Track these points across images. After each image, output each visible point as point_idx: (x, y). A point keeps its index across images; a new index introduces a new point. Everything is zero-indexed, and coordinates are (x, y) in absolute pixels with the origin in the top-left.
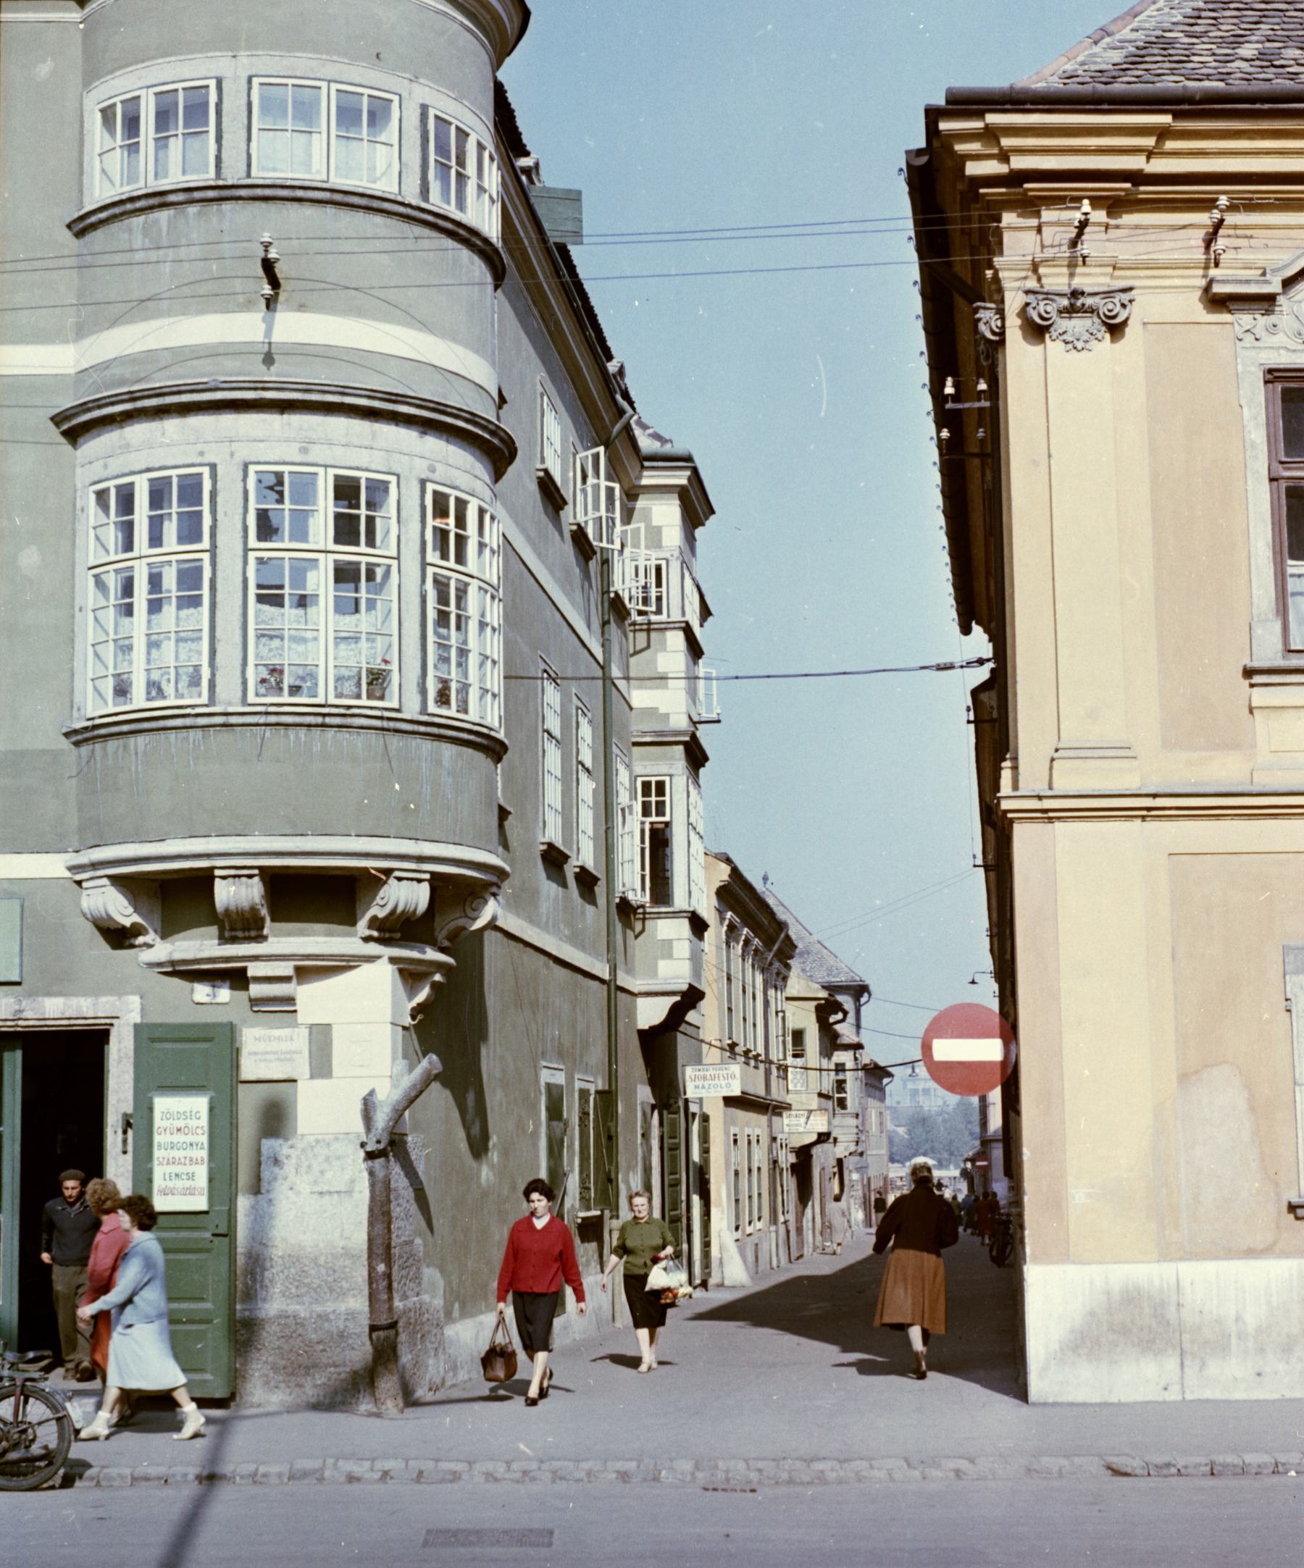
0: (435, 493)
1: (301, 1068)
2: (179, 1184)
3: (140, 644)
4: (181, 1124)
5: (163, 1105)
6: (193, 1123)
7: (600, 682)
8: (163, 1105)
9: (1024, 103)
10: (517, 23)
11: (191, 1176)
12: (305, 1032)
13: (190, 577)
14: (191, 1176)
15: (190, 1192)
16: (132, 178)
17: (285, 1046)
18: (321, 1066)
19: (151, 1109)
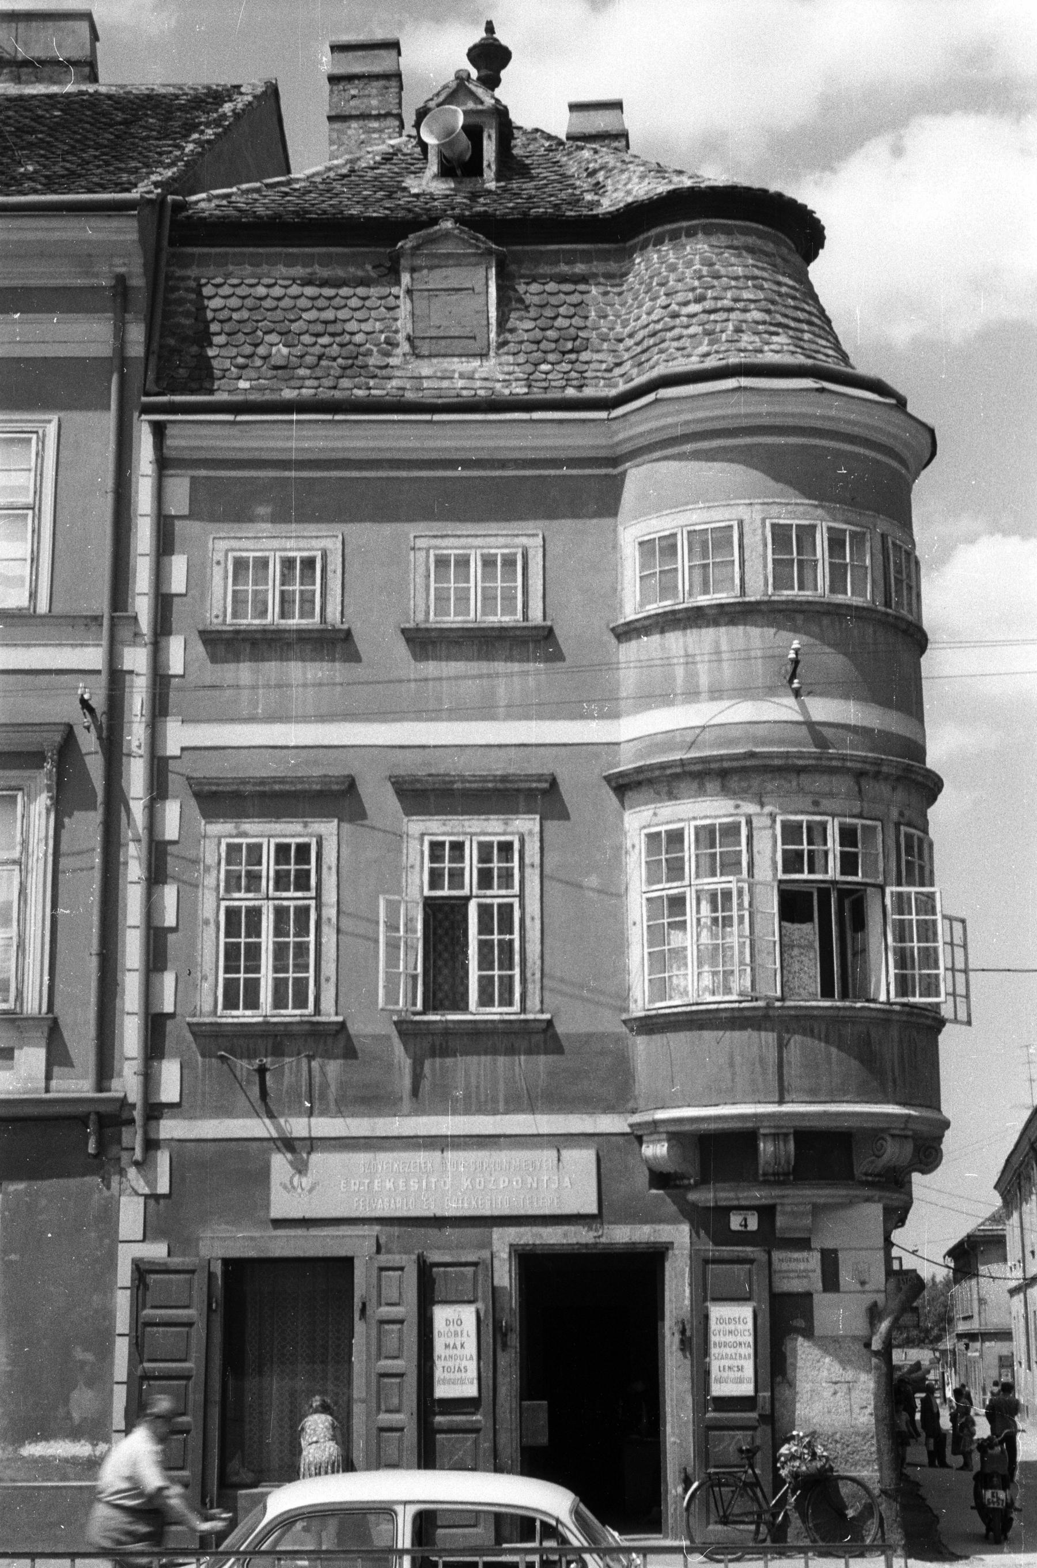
0: (906, 834)
1: (816, 1282)
2: (732, 1375)
3: (267, 884)
4: (732, 1327)
5: (718, 1312)
6: (740, 1327)
7: (971, 967)
8: (718, 1312)
9: (743, 612)
10: (928, 456)
11: (740, 1369)
12: (817, 1255)
13: (452, 873)
14: (740, 1369)
15: (740, 1381)
16: (668, 589)
17: (802, 1266)
18: (831, 1282)
19: (707, 1317)
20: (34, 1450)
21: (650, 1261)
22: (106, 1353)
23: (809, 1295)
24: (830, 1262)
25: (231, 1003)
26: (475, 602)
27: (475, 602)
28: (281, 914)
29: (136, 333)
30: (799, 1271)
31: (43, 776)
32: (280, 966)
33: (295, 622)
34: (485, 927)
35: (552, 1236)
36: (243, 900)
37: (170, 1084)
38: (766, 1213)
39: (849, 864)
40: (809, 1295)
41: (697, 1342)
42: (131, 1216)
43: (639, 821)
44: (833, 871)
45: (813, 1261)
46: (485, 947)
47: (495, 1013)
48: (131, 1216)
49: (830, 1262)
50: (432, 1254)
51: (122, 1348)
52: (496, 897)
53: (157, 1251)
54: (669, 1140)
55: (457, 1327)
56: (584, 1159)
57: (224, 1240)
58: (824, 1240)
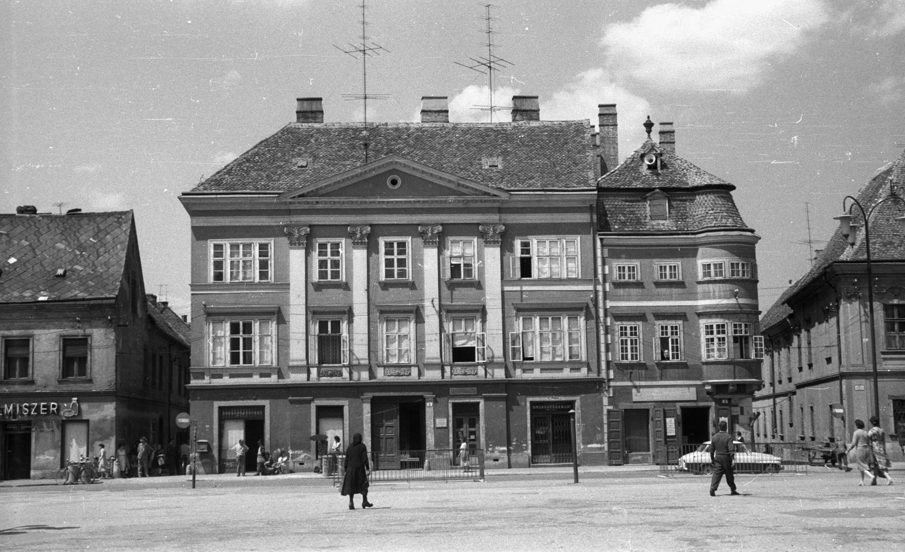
18: (742, 413)
20: (590, 446)
21: (707, 409)
22: (602, 427)
23: (737, 416)
25: (623, 359)
28: (632, 341)
29: (595, 217)
32: (632, 351)
34: (672, 343)
36: (624, 338)
37: (612, 376)
38: (729, 400)
40: (737, 416)
42: (605, 401)
44: (743, 334)
47: (675, 360)
48: (605, 401)
49: (742, 409)
50: (665, 408)
51: (606, 427)
52: (675, 337)
53: (611, 408)
55: (671, 422)
56: (693, 389)
57: (624, 405)
58: (740, 405)
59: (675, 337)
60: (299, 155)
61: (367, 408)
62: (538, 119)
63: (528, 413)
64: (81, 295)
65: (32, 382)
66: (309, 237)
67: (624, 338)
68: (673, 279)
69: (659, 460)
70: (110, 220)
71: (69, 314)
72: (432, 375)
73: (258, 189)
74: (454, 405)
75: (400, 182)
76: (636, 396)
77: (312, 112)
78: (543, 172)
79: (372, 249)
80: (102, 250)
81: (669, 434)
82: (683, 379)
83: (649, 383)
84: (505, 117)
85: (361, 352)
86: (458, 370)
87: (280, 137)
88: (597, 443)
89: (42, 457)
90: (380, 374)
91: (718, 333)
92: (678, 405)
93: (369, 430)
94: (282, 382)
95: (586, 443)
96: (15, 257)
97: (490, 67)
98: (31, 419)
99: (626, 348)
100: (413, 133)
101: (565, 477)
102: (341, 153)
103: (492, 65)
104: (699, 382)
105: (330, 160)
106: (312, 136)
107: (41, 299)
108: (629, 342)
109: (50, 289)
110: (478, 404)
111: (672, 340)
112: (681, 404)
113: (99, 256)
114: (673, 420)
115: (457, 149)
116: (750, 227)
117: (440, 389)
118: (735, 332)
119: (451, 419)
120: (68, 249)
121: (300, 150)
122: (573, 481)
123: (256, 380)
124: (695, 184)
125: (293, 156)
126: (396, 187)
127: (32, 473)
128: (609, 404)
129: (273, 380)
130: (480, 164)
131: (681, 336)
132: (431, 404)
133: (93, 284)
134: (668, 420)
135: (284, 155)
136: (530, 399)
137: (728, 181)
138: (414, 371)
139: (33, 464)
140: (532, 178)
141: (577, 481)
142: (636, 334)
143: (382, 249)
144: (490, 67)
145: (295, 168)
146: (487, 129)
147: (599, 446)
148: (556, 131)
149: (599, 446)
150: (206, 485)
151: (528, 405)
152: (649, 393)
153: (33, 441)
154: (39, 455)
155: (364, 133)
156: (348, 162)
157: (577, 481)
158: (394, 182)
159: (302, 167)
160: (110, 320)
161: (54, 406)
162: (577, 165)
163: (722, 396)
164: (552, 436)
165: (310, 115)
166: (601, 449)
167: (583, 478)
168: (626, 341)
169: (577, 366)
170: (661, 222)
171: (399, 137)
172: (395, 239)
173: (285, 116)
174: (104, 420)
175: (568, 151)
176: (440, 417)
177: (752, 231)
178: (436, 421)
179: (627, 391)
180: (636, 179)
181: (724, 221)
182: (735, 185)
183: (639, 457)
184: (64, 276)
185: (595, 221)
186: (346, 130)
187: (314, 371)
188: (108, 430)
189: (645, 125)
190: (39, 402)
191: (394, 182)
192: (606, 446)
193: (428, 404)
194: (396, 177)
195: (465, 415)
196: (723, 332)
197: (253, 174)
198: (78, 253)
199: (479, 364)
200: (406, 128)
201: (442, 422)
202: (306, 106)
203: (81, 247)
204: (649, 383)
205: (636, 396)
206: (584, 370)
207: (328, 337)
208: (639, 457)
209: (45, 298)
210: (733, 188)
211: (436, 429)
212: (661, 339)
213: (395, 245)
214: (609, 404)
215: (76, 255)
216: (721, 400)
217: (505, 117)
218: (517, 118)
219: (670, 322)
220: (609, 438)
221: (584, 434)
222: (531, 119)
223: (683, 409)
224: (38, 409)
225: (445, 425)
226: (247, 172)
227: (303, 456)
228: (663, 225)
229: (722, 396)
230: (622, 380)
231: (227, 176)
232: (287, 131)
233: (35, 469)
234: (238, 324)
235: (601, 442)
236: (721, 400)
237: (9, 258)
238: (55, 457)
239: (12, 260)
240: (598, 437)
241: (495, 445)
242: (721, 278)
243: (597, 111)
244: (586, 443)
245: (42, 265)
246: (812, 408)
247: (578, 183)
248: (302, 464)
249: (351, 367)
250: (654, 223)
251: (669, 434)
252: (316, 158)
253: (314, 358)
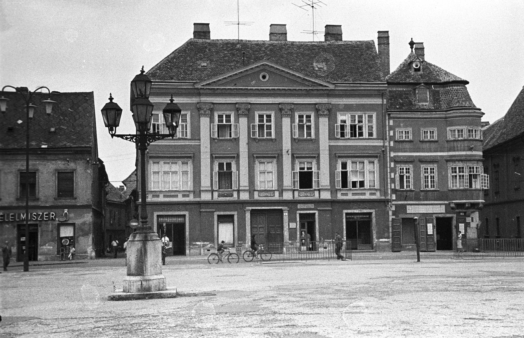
1: (471, 221)
18: (472, 221)
20: (381, 240)
21: (451, 219)
22: (389, 229)
23: (470, 223)
24: (472, 218)
25: (425, 187)
26: (429, 137)
27: (429, 137)
28: (431, 176)
29: (385, 100)
30: (468, 220)
31: (275, 160)
32: (431, 183)
33: (407, 139)
34: (407, 178)
35: (440, 215)
36: (426, 175)
37: (394, 198)
38: (465, 213)
39: (476, 172)
40: (470, 223)
41: (457, 227)
42: (390, 213)
43: (451, 165)
44: (475, 173)
45: (470, 218)
46: (407, 181)
47: (433, 189)
48: (390, 213)
49: (472, 218)
50: (426, 217)
51: (390, 229)
52: (432, 175)
53: (394, 217)
54: (93, 211)
55: (430, 226)
56: (444, 206)
57: (402, 216)
58: (472, 216)
59: (432, 175)
60: (201, 59)
61: (248, 215)
62: (341, 40)
63: (344, 220)
64: (68, 144)
65: (38, 199)
66: (212, 110)
67: (426, 175)
68: (432, 139)
69: (395, 249)
70: (80, 98)
71: (62, 157)
72: (288, 196)
73: (179, 80)
74: (300, 214)
75: (267, 77)
76: (410, 210)
77: (204, 32)
78: (351, 73)
79: (251, 119)
80: (77, 116)
81: (429, 233)
82: (437, 201)
83: (417, 202)
84: (320, 38)
85: (244, 182)
86: (303, 194)
87: (187, 48)
88: (385, 238)
89: (44, 247)
90: (256, 196)
91: (460, 172)
92: (434, 216)
93: (250, 230)
94: (198, 199)
95: (378, 238)
96: (21, 120)
97: (313, 7)
98: (38, 222)
99: (428, 181)
100: (268, 47)
101: (411, 258)
102: (226, 58)
103: (314, 5)
104: (446, 202)
105: (220, 62)
106: (206, 47)
107: (43, 146)
108: (429, 178)
109: (47, 142)
110: (315, 214)
111: (406, 176)
112: (435, 215)
113: (76, 120)
114: (431, 225)
115: (296, 57)
116: (478, 107)
117: (292, 204)
118: (470, 171)
119: (298, 223)
120: (55, 115)
121: (201, 56)
122: (416, 260)
123: (367, 197)
124: (445, 80)
125: (197, 60)
126: (266, 80)
127: (39, 257)
128: (393, 215)
129: (191, 198)
130: (313, 67)
131: (436, 175)
132: (287, 214)
133: (75, 138)
134: (428, 225)
135: (191, 59)
136: (345, 211)
137: (464, 78)
138: (277, 194)
139: (39, 251)
140: (346, 76)
141: (419, 261)
142: (409, 173)
143: (257, 119)
144: (313, 7)
145: (200, 67)
146: (313, 45)
147: (386, 240)
148: (355, 47)
149: (386, 240)
150: (172, 263)
151: (344, 215)
152: (415, 209)
153: (39, 236)
154: (43, 246)
155: (238, 46)
156: (232, 64)
157: (419, 261)
158: (264, 77)
159: (204, 66)
160: (88, 161)
161: (53, 215)
162: (371, 68)
163: (461, 210)
164: (358, 235)
165: (202, 34)
166: (388, 242)
167: (422, 258)
168: (428, 176)
169: (373, 192)
170: (424, 104)
171: (260, 49)
172: (265, 113)
173: (189, 35)
174: (84, 224)
175: (365, 59)
176: (292, 222)
177: (480, 110)
178: (290, 225)
179: (404, 207)
180: (409, 77)
181: (464, 103)
182: (468, 80)
183: (410, 247)
184: (54, 132)
185: (385, 103)
186: (227, 44)
187: (216, 194)
188: (86, 228)
189: (409, 44)
190: (43, 211)
191: (264, 77)
192: (390, 240)
193: (285, 214)
194: (263, 74)
195: (308, 222)
196: (463, 172)
197: (175, 70)
198: (62, 118)
199: (315, 190)
200: (263, 44)
201: (293, 225)
202: (199, 29)
203: (64, 114)
204: (417, 202)
205: (410, 210)
206: (378, 193)
207: (225, 172)
208: (410, 247)
209: (46, 146)
210: (467, 83)
211: (290, 229)
212: (400, 175)
213: (224, 117)
214: (393, 215)
215: (60, 119)
216: (460, 212)
217: (320, 38)
218: (329, 38)
219: (429, 165)
220: (393, 235)
221: (377, 233)
222: (337, 40)
223: (438, 219)
224: (42, 216)
225: (295, 227)
226: (171, 69)
227: (209, 246)
228: (426, 105)
229: (461, 210)
230: (400, 201)
231: (158, 71)
232: (189, 43)
233: (40, 255)
234: (223, 163)
235: (388, 238)
236: (460, 212)
237: (18, 120)
238: (54, 247)
239: (20, 122)
240: (386, 235)
241: (324, 239)
242: (462, 138)
243: (377, 35)
244: (378, 238)
245: (39, 125)
246: (497, 219)
247: (375, 79)
248: (208, 250)
249: (238, 191)
250: (420, 104)
251: (429, 233)
252: (211, 61)
253: (216, 187)
